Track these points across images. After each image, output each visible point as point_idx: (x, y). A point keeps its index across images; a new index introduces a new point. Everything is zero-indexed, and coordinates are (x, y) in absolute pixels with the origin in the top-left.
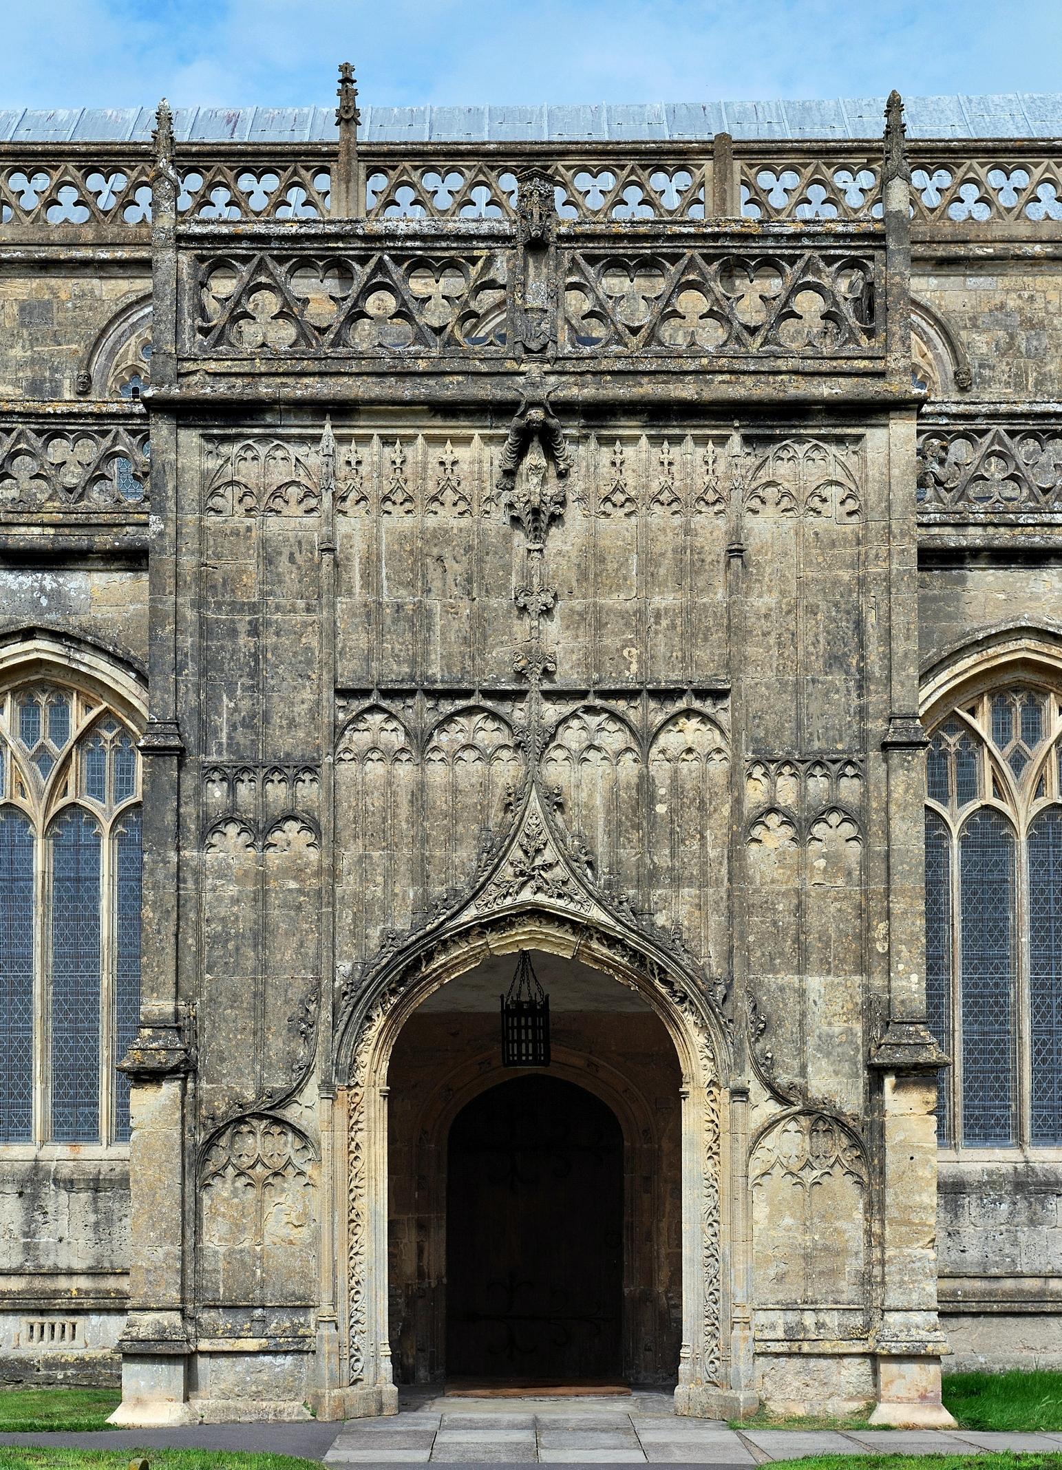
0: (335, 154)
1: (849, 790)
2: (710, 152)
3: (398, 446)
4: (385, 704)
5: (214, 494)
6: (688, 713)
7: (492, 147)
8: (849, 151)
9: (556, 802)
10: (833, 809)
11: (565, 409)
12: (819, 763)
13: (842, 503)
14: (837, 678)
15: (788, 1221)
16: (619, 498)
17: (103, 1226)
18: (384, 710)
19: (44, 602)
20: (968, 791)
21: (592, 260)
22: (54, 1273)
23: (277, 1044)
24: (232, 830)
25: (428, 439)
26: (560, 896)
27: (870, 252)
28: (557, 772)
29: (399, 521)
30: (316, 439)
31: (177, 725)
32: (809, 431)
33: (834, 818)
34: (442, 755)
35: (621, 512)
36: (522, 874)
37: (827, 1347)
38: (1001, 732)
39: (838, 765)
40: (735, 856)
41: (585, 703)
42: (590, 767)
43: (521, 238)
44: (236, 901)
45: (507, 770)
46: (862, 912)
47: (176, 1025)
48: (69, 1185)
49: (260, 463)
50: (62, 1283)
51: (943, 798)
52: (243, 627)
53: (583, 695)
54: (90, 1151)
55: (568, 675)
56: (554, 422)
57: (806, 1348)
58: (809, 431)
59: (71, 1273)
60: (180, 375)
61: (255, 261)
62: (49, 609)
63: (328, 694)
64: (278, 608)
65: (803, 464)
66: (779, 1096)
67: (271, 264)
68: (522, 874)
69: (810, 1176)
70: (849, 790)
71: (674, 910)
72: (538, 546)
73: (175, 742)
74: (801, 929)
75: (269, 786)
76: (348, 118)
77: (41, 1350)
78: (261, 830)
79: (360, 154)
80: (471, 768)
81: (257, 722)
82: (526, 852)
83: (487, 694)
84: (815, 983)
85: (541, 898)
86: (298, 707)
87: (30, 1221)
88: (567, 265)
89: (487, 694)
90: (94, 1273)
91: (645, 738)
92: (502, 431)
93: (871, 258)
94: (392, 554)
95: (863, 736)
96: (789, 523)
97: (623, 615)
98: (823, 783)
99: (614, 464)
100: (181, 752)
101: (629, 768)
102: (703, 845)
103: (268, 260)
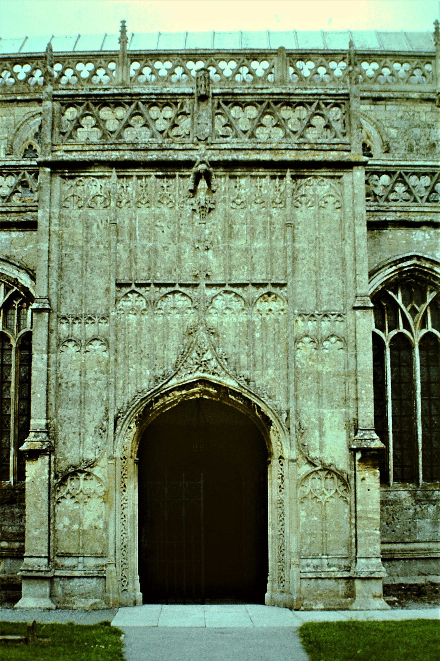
0: (117, 55)
2: (277, 54)
3: (144, 180)
4: (137, 289)
5: (66, 200)
10: (332, 336)
11: (215, 164)
12: (326, 315)
13: (334, 203)
16: (239, 201)
18: (137, 292)
20: (394, 325)
21: (226, 103)
24: (70, 345)
25: (157, 177)
26: (214, 374)
27: (344, 101)
28: (213, 319)
30: (109, 177)
31: (48, 299)
32: (319, 174)
33: (333, 339)
34: (162, 312)
35: (239, 207)
36: (197, 363)
39: (335, 316)
41: (224, 289)
51: (382, 329)
53: (223, 285)
56: (211, 169)
58: (319, 174)
60: (53, 151)
61: (85, 105)
63: (113, 286)
66: (311, 463)
67: (91, 106)
68: (197, 363)
70: (339, 328)
72: (204, 222)
73: (47, 306)
75: (87, 325)
76: (123, 40)
79: (128, 55)
82: (199, 354)
83: (181, 285)
85: (206, 375)
88: (216, 105)
89: (181, 285)
92: (188, 173)
93: (344, 104)
99: (236, 187)
100: (49, 311)
103: (90, 104)
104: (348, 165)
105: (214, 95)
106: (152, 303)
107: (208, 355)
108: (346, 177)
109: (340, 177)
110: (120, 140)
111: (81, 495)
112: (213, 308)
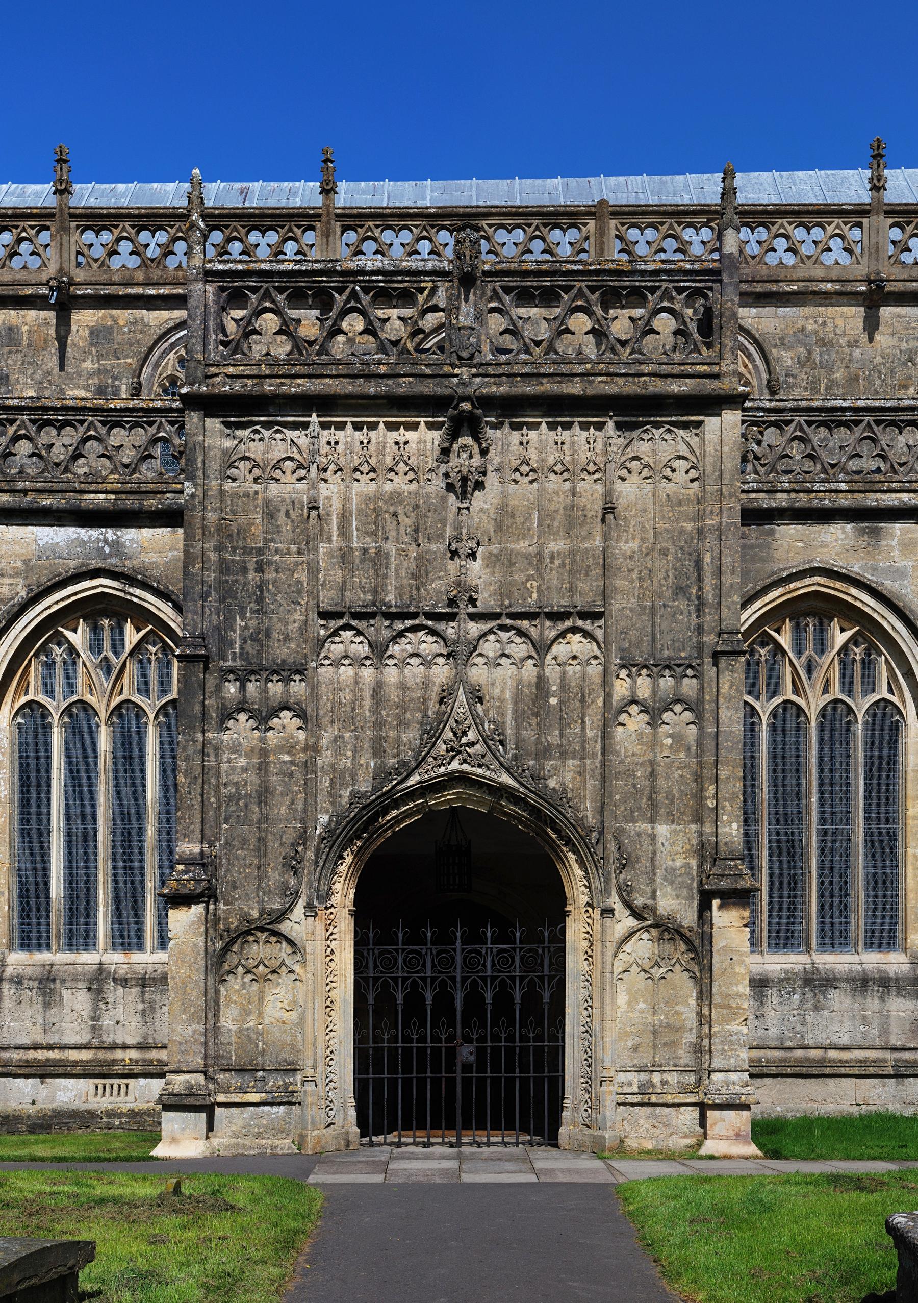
1: (689, 686)
4: (354, 623)
5: (231, 466)
6: (574, 630)
7: (432, 210)
8: (694, 213)
9: (477, 696)
11: (487, 402)
12: (668, 667)
14: (681, 604)
15: (642, 1006)
17: (148, 1012)
19: (107, 549)
20: (774, 691)
22: (113, 1047)
23: (274, 876)
26: (480, 766)
27: (709, 284)
28: (478, 673)
29: (365, 487)
35: (526, 480)
37: (669, 1099)
38: (95, 647)
39: (682, 668)
40: (606, 736)
42: (502, 670)
43: (456, 273)
44: (245, 770)
45: (442, 672)
46: (698, 778)
47: (200, 862)
48: (124, 982)
49: (269, 444)
50: (119, 1054)
51: (756, 695)
52: (251, 566)
53: (497, 616)
54: (137, 957)
55: (486, 601)
57: (654, 1099)
59: (125, 1047)
62: (110, 555)
64: (277, 551)
65: (660, 444)
69: (657, 972)
70: (689, 686)
71: (562, 776)
74: (653, 790)
77: (104, 1104)
78: (263, 717)
79: (337, 215)
80: (415, 671)
81: (260, 637)
84: (662, 830)
86: (292, 621)
87: (96, 1009)
90: (141, 1047)
91: (541, 649)
93: (710, 289)
94: (360, 511)
95: (700, 647)
96: (648, 487)
97: (527, 556)
98: (671, 681)
99: (521, 443)
101: (530, 670)
102: (583, 729)
103: (272, 290)
104: (713, 404)
105: (485, 273)
106: (379, 651)
107: (472, 736)
108: (711, 423)
109: (699, 424)
110: (324, 357)
111: (261, 968)
112: (481, 655)
